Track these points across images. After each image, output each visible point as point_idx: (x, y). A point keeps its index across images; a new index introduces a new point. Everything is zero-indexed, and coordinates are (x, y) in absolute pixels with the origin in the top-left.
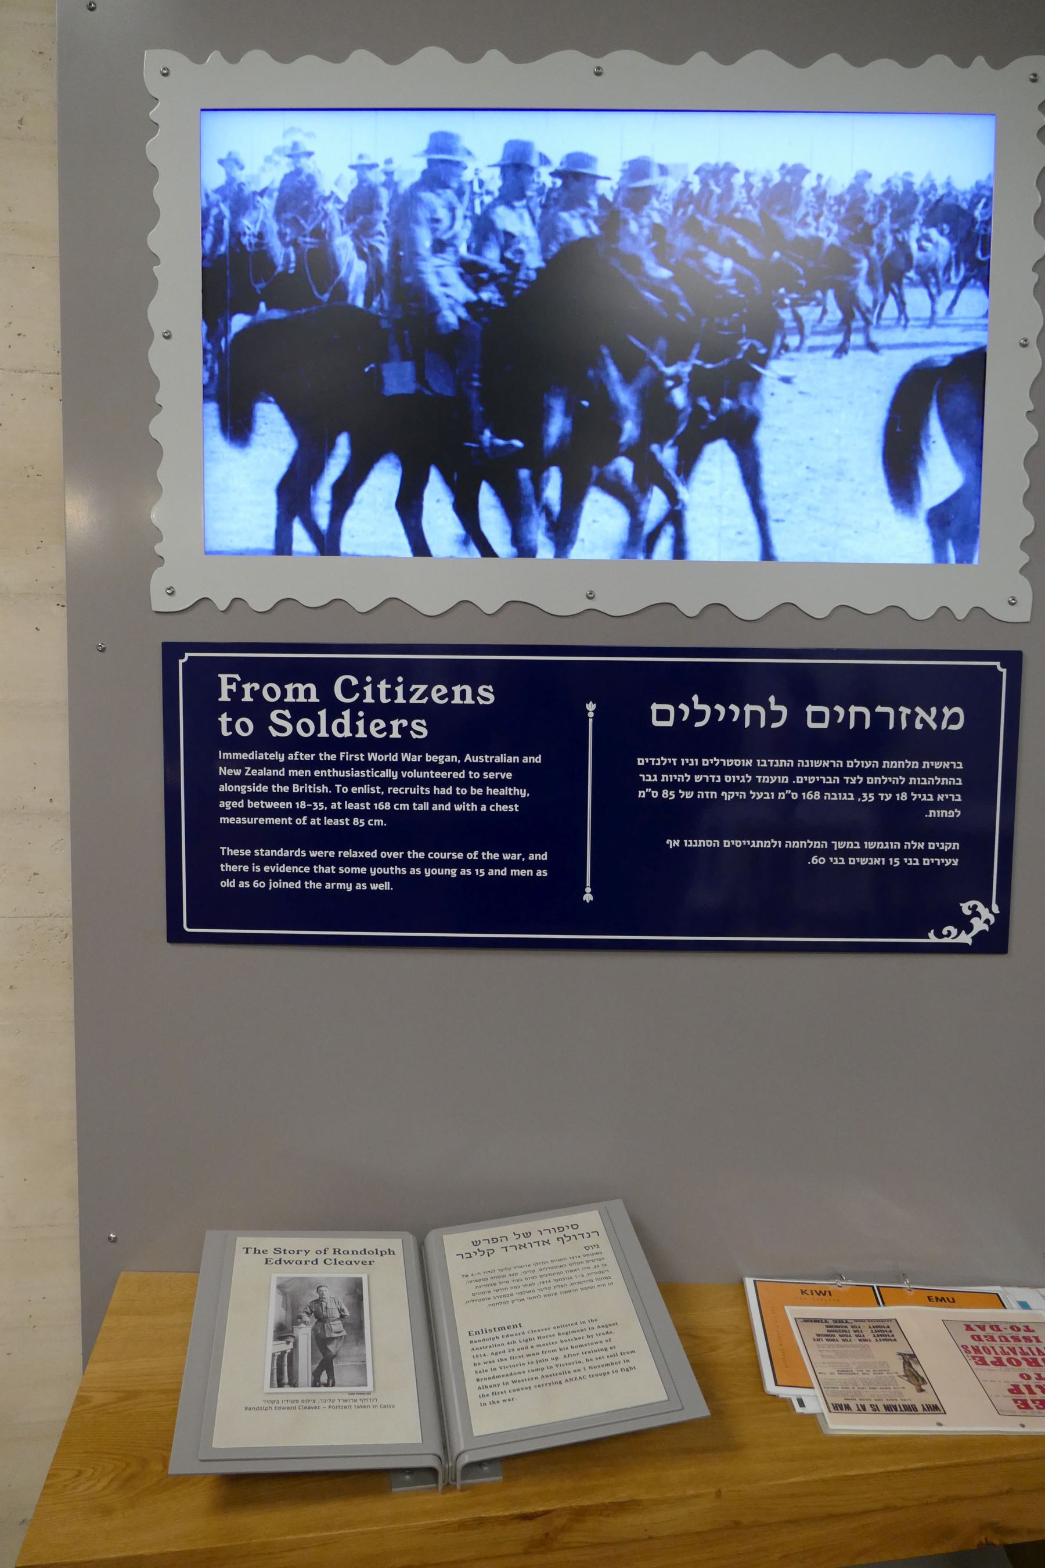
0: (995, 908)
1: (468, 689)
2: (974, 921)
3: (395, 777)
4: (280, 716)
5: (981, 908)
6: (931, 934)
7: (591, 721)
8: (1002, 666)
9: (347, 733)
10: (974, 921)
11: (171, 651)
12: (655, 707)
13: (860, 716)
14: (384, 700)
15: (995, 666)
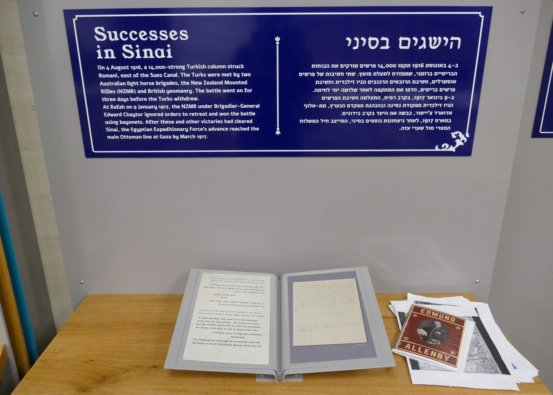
0: (468, 135)
1: (115, 33)
2: (457, 141)
3: (239, 76)
4: (127, 48)
5: (461, 135)
6: (437, 147)
7: (278, 46)
8: (482, 14)
9: (163, 56)
10: (457, 141)
11: (69, 14)
12: (401, 39)
13: (456, 42)
14: (423, 39)
15: (478, 15)
